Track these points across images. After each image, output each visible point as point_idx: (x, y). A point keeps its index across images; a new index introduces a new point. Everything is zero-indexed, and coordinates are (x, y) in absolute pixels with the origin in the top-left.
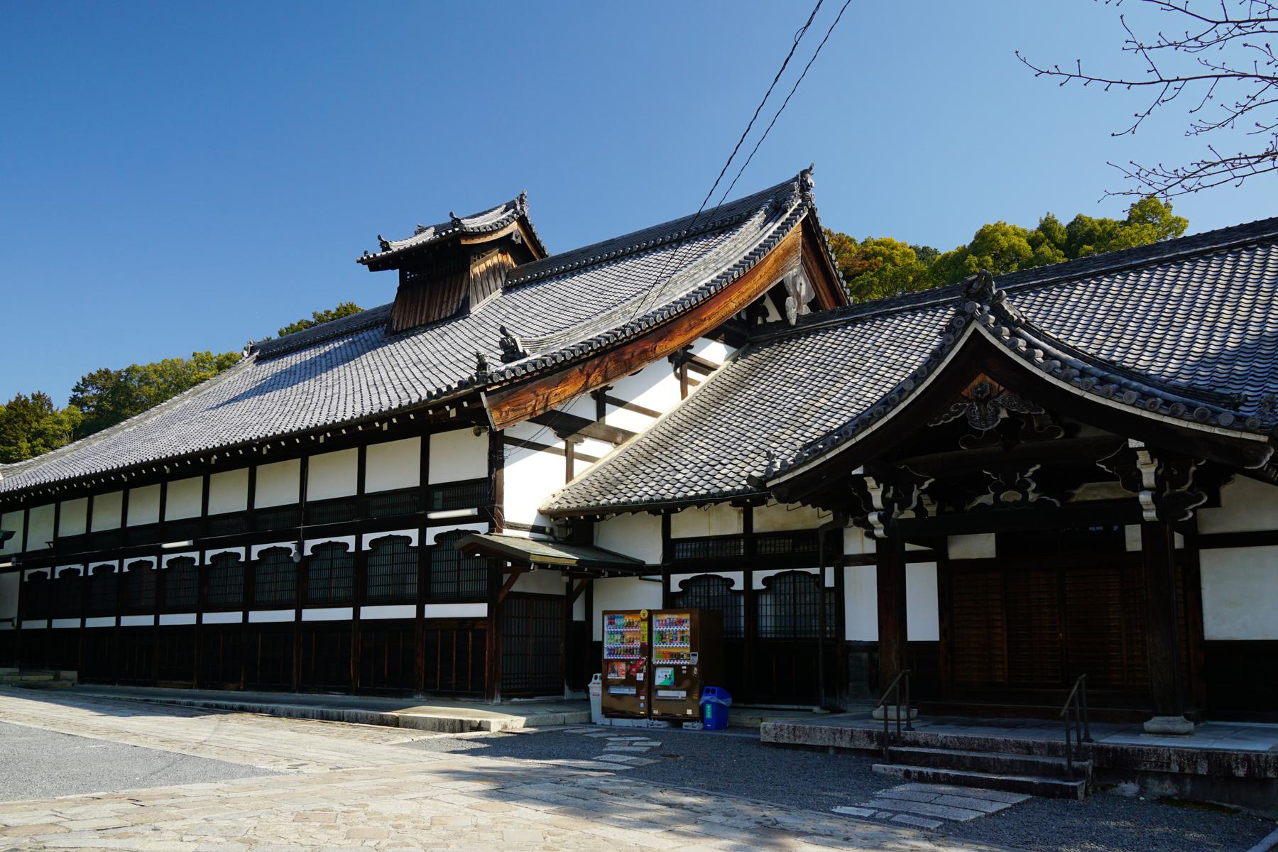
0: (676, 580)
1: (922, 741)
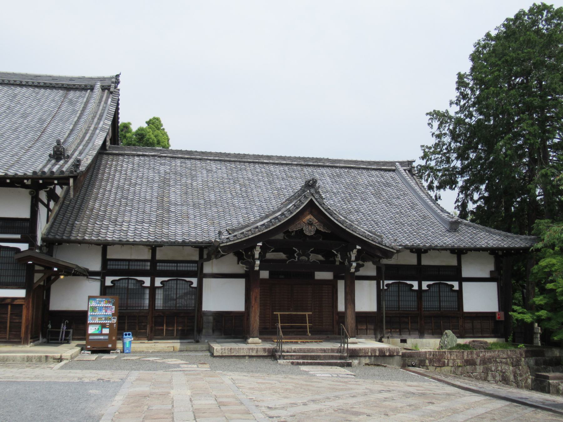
0: (109, 281)
1: (286, 350)
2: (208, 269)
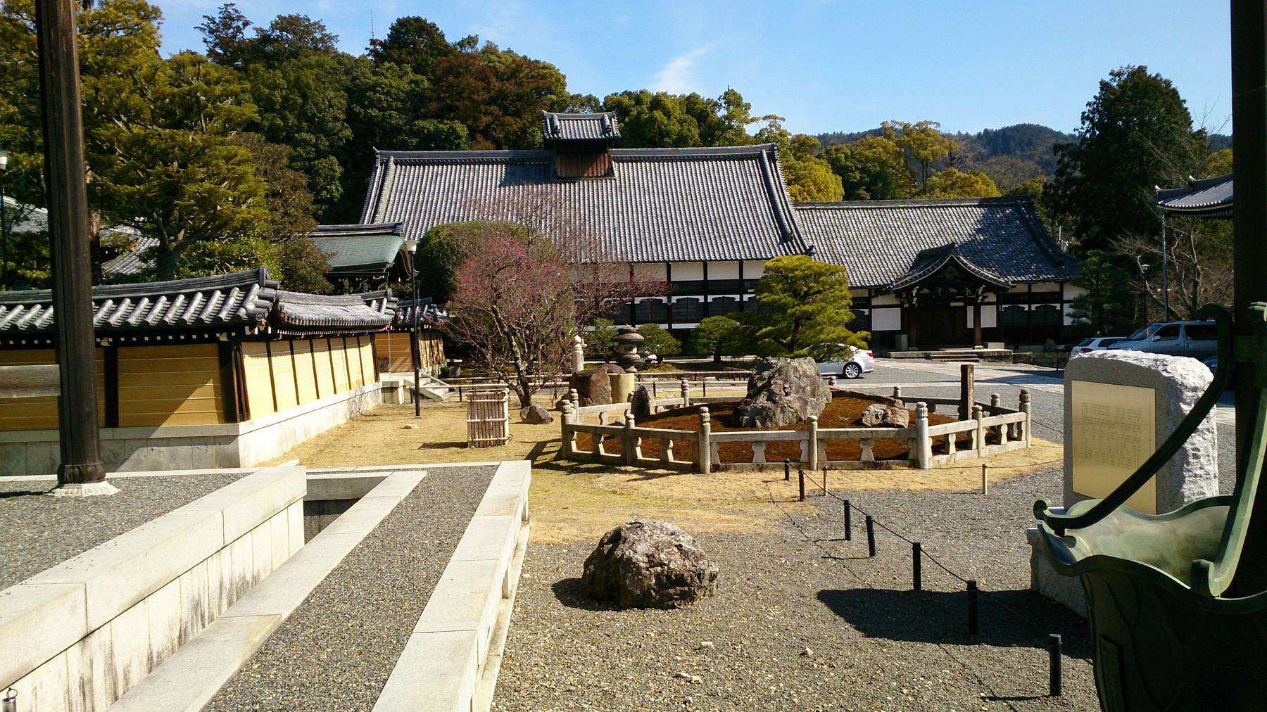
2: (875, 302)
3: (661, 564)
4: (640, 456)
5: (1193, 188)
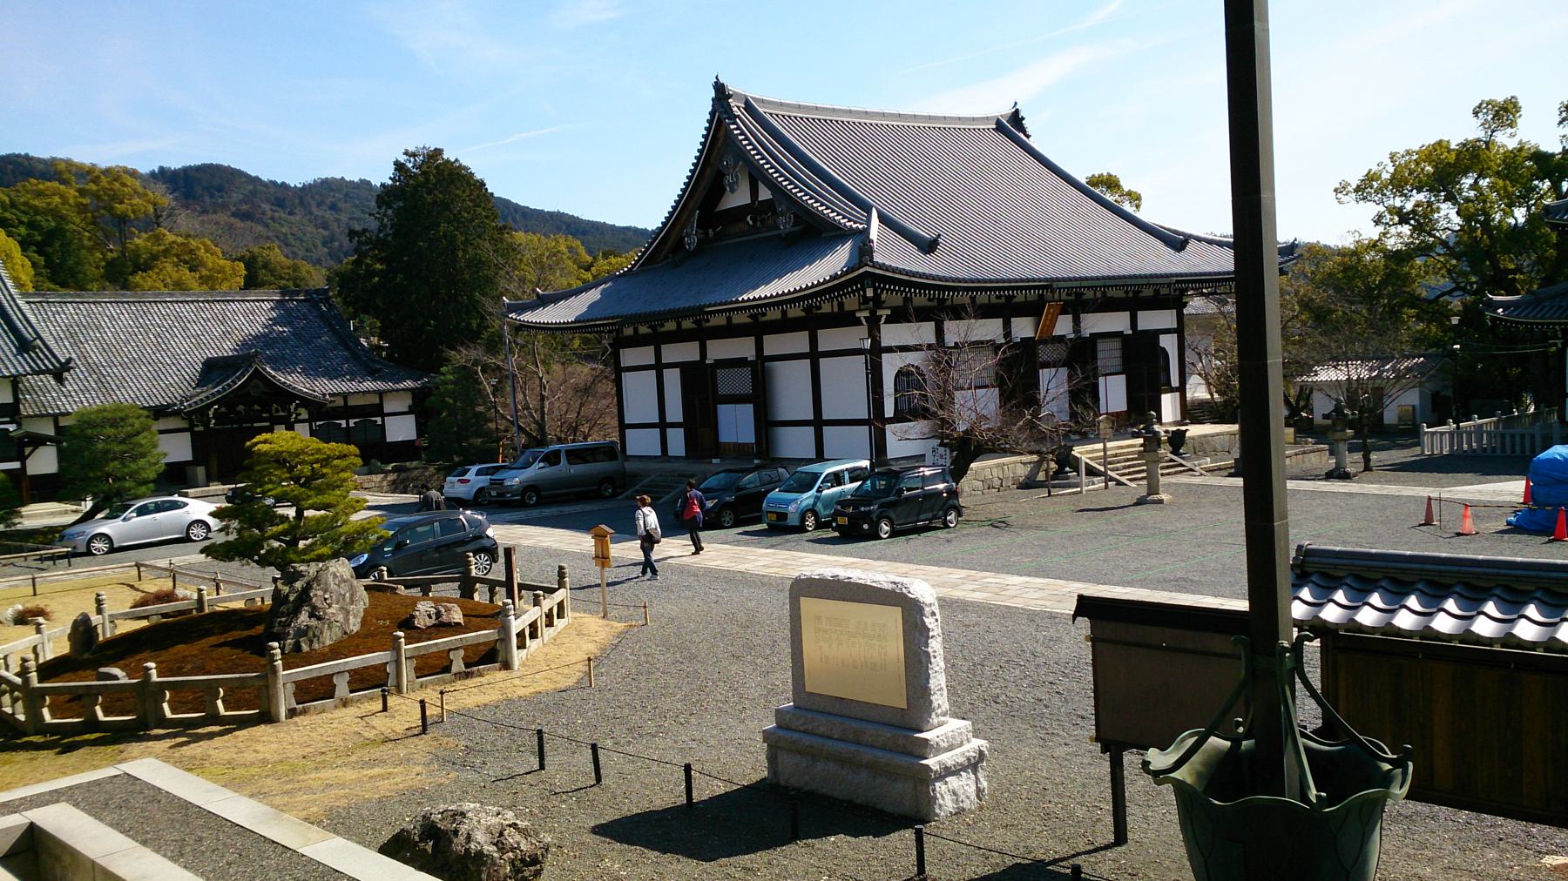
3: (513, 849)
4: (168, 714)
5: (543, 302)
